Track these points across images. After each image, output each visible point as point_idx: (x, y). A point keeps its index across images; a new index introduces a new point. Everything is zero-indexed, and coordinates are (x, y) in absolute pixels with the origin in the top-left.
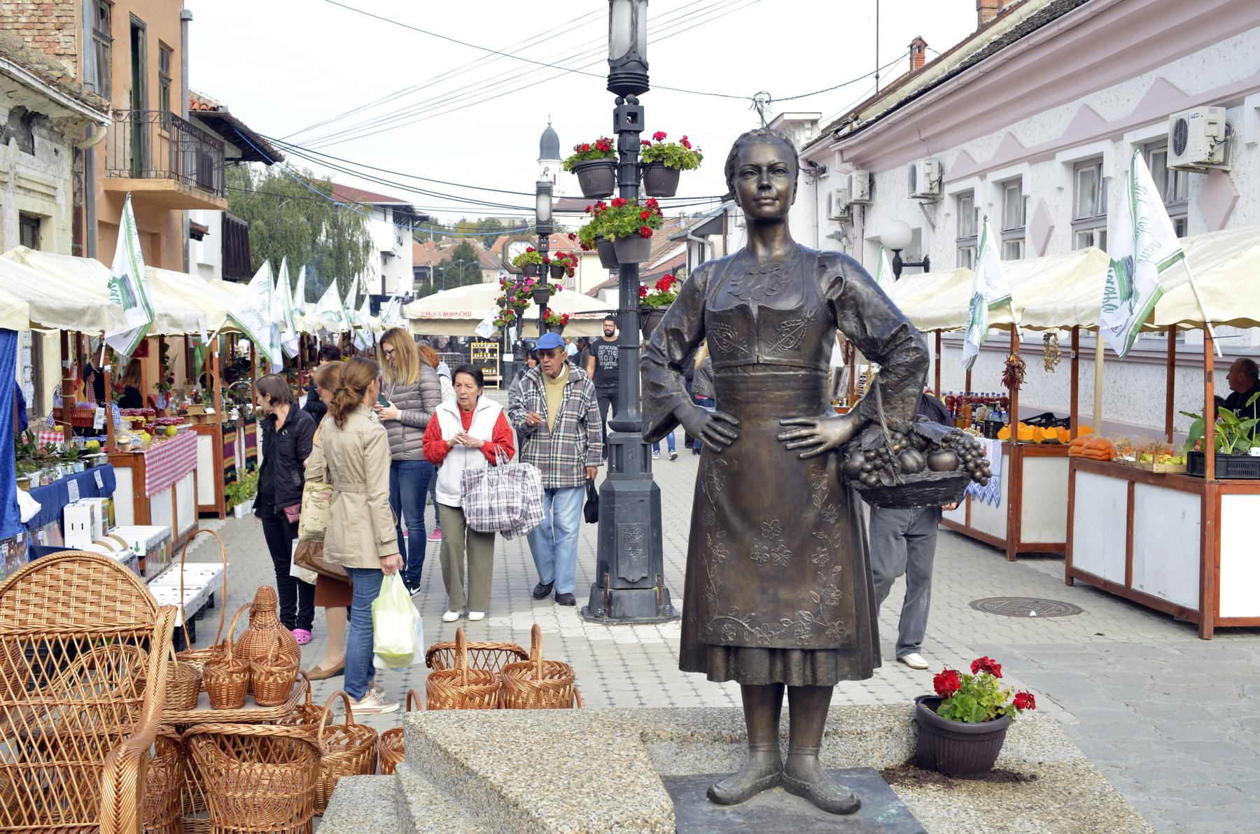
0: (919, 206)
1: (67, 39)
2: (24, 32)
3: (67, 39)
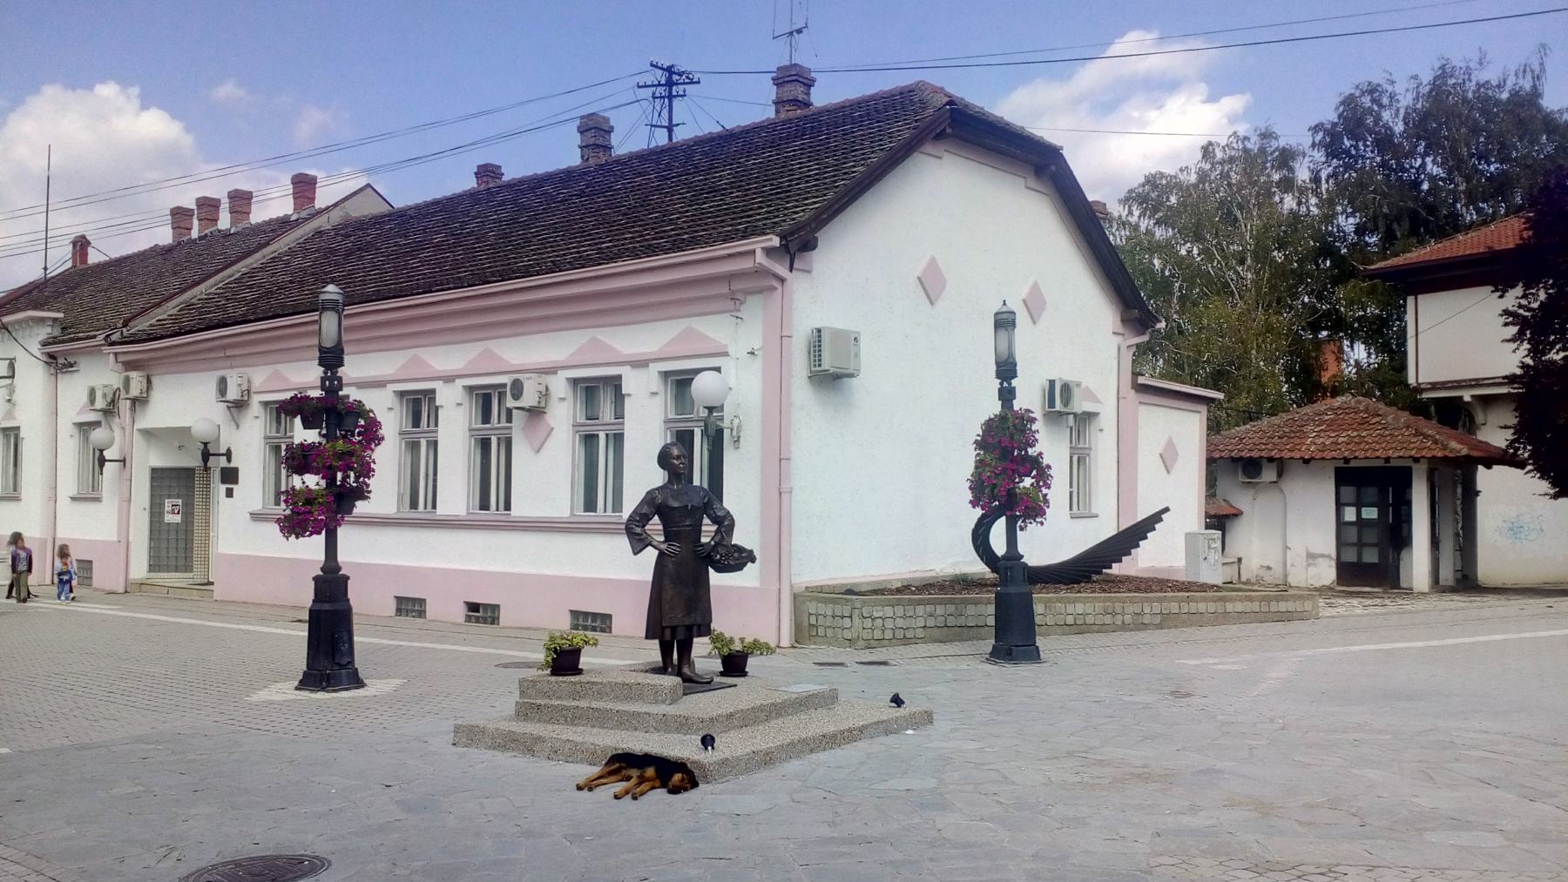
0: (226, 409)
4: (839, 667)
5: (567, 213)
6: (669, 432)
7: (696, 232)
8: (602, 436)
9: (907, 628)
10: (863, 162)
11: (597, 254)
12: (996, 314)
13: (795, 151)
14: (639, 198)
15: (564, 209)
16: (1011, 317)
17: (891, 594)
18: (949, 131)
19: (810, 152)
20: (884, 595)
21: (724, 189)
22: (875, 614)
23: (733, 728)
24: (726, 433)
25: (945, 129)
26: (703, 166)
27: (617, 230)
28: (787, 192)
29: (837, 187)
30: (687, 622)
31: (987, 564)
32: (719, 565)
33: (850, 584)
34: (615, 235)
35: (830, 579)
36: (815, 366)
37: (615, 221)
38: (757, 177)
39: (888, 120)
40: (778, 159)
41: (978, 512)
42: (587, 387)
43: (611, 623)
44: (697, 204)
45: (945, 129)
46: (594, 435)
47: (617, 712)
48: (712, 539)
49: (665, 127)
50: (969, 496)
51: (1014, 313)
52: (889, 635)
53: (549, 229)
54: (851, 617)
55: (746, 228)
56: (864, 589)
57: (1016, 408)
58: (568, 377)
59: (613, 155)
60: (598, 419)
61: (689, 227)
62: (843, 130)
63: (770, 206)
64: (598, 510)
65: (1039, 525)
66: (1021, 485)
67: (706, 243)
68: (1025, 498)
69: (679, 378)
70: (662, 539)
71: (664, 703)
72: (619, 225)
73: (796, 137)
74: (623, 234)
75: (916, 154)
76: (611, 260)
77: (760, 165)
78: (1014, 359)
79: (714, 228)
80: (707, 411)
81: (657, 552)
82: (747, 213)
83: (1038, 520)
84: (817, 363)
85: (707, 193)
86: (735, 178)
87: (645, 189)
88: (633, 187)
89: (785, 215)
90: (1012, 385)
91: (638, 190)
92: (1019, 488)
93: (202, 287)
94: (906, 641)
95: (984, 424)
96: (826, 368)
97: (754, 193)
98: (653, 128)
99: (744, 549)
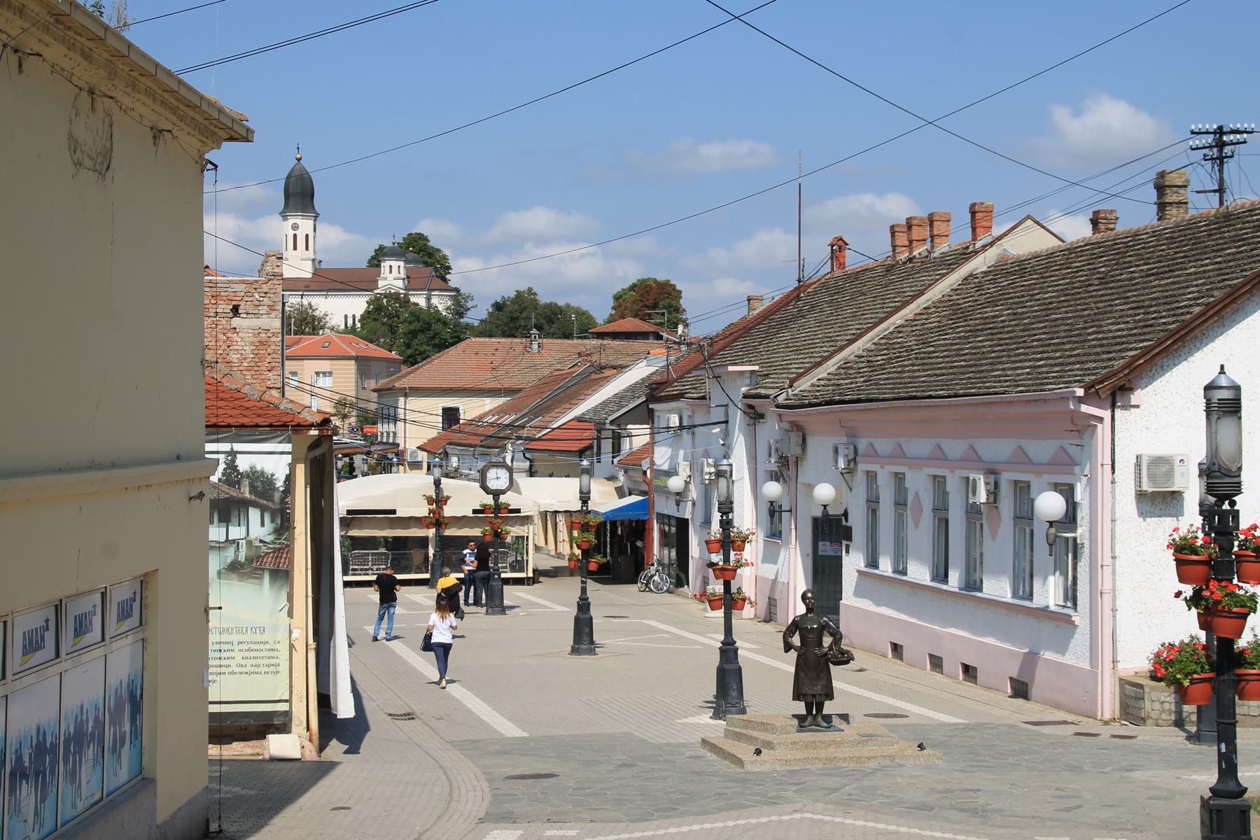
1: (275, 377)
2: (245, 373)
3: (275, 377)
93: (860, 343)
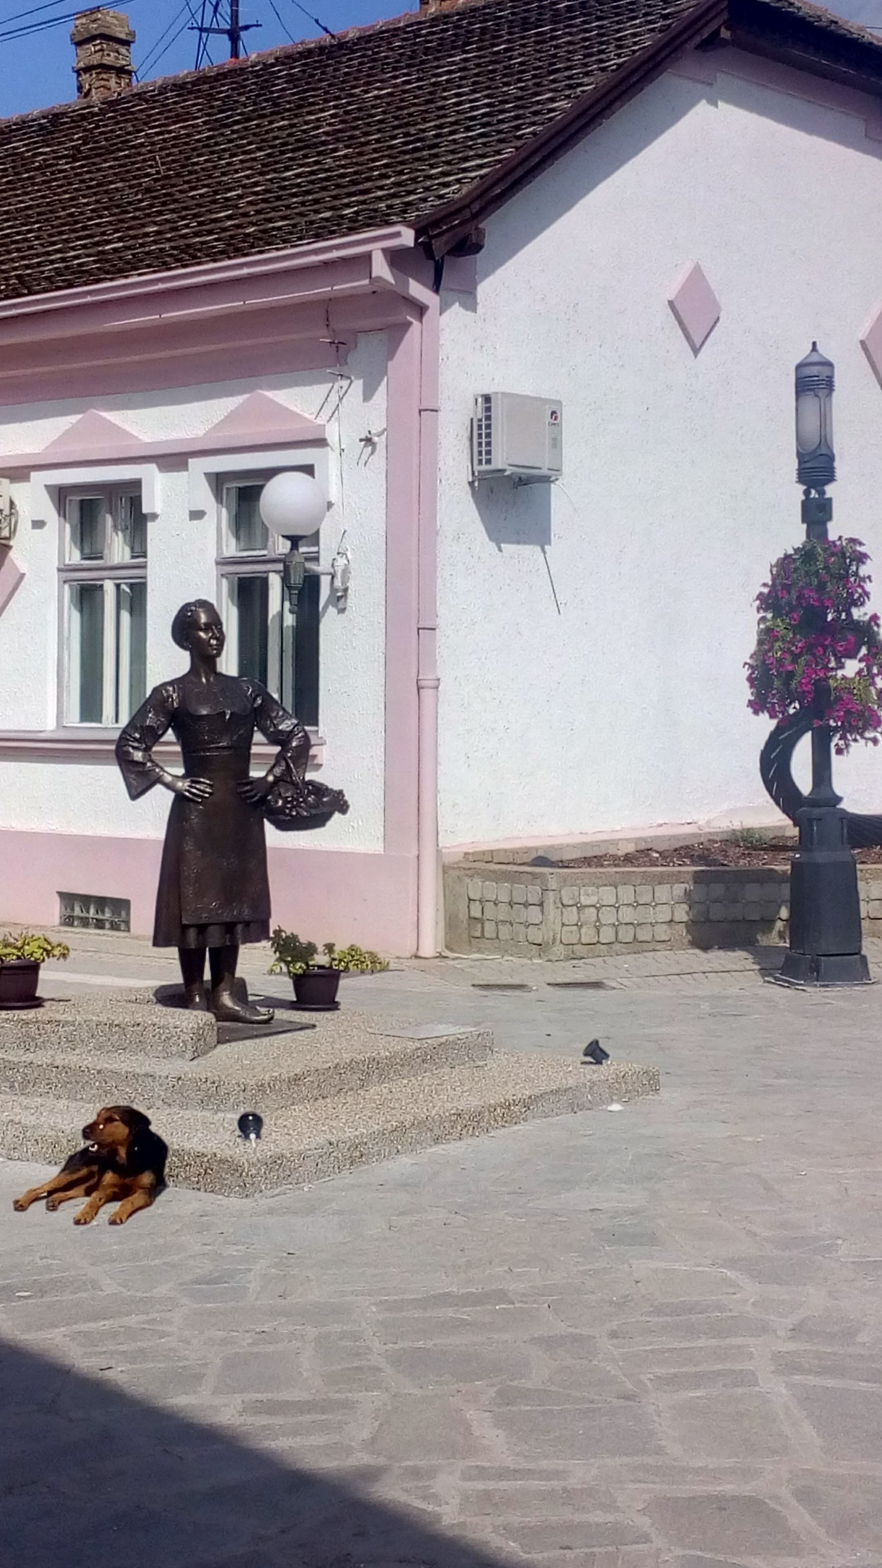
4: (517, 993)
5: (49, 188)
6: (66, 587)
7: (270, 220)
8: (109, 587)
9: (639, 925)
10: (567, 93)
11: (95, 262)
12: (799, 367)
13: (450, 72)
14: (174, 161)
15: (44, 182)
16: (824, 371)
17: (615, 866)
18: (725, 34)
19: (477, 75)
20: (602, 866)
21: (324, 143)
22: (585, 900)
23: (302, 1101)
24: (325, 581)
25: (717, 31)
26: (289, 102)
27: (134, 218)
28: (431, 147)
29: (519, 138)
30: (226, 918)
31: (785, 811)
32: (282, 817)
33: (542, 848)
34: (129, 228)
35: (507, 839)
36: (480, 462)
37: (130, 203)
38: (381, 122)
39: (617, 15)
40: (419, 88)
41: (766, 724)
42: (82, 501)
43: (128, 914)
44: (275, 171)
45: (717, 31)
46: (95, 585)
47: (99, 1072)
48: (270, 771)
49: (223, 31)
50: (747, 693)
51: (830, 365)
52: (607, 935)
53: (16, 219)
54: (541, 905)
55: (357, 213)
56: (567, 856)
57: (832, 536)
58: (49, 483)
59: (134, 83)
60: (101, 558)
61: (258, 212)
62: (538, 34)
63: (401, 173)
64: (104, 718)
65: (870, 744)
66: (840, 673)
67: (285, 241)
68: (845, 696)
69: (241, 485)
70: (181, 771)
71: (182, 1057)
72: (136, 209)
73: (454, 48)
74: (143, 226)
75: (665, 75)
76: (121, 272)
77: (388, 100)
78: (830, 449)
79: (301, 214)
80: (288, 544)
81: (171, 795)
82: (361, 187)
83: (868, 735)
84: (484, 457)
85: (293, 151)
86: (342, 122)
87: (186, 143)
88: (164, 140)
89: (427, 189)
90: (827, 496)
91: (174, 146)
92: (834, 678)
94: (637, 946)
95: (777, 565)
96: (500, 467)
97: (375, 151)
98: (204, 35)
99: (327, 789)
